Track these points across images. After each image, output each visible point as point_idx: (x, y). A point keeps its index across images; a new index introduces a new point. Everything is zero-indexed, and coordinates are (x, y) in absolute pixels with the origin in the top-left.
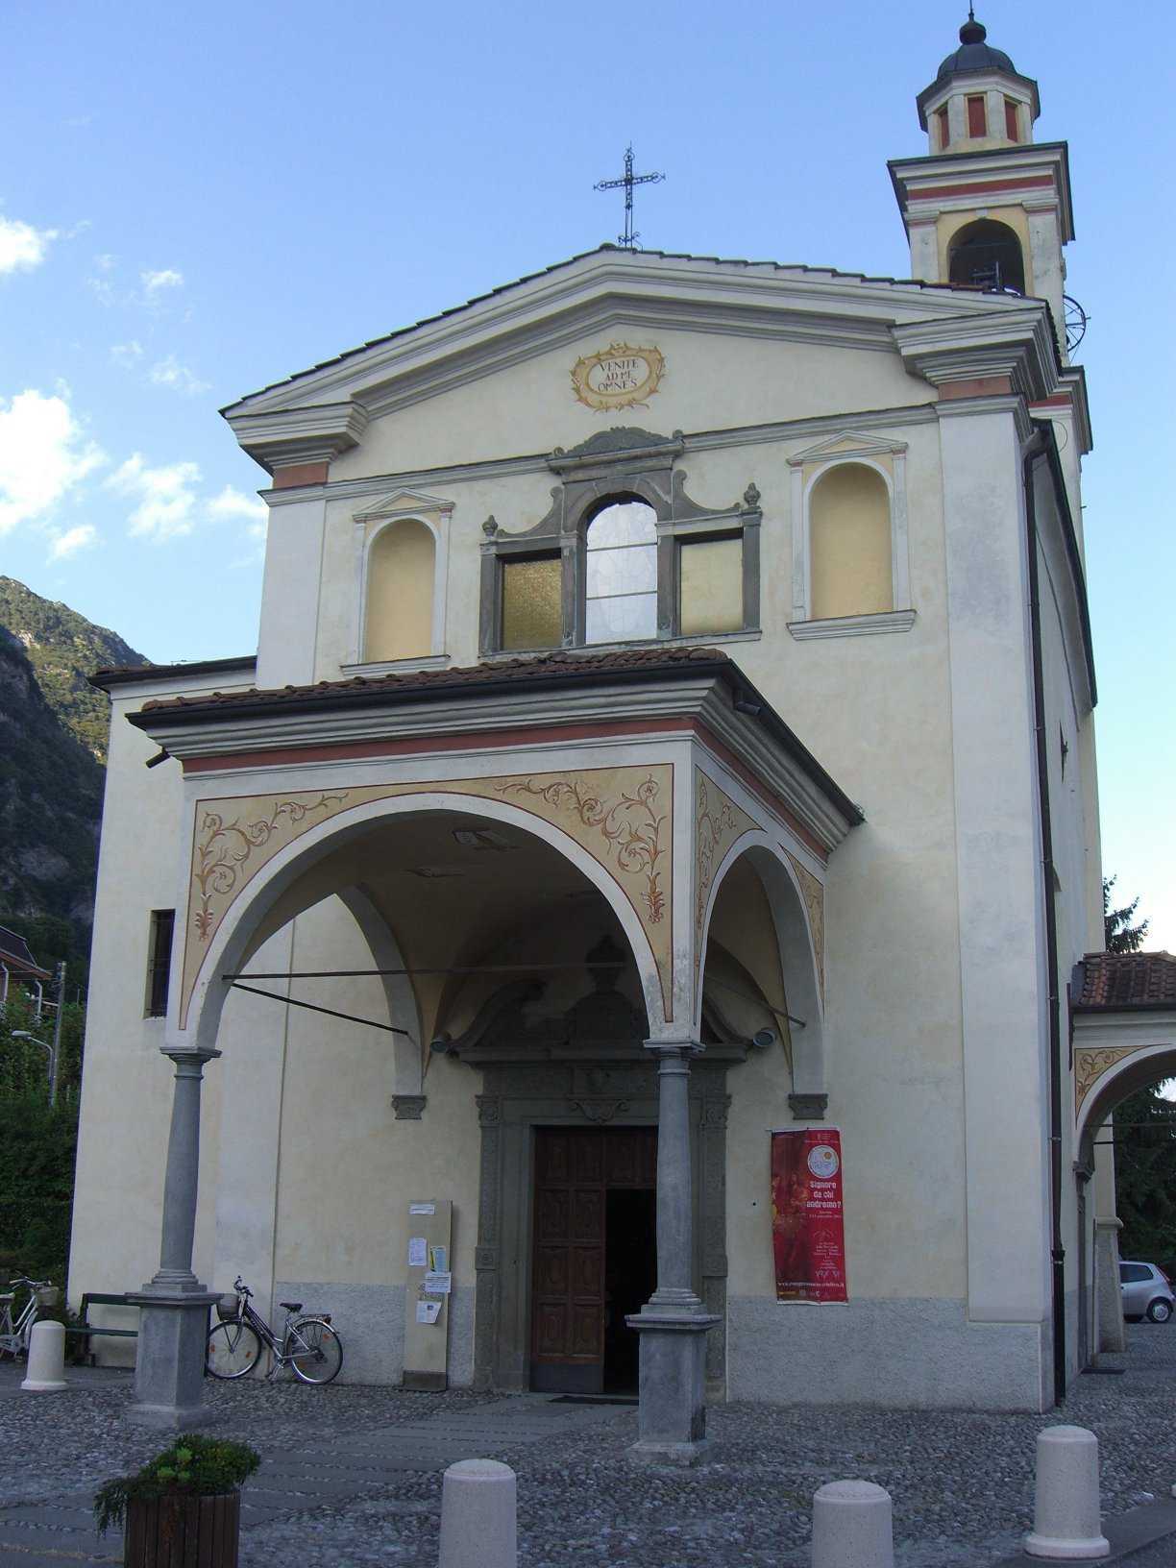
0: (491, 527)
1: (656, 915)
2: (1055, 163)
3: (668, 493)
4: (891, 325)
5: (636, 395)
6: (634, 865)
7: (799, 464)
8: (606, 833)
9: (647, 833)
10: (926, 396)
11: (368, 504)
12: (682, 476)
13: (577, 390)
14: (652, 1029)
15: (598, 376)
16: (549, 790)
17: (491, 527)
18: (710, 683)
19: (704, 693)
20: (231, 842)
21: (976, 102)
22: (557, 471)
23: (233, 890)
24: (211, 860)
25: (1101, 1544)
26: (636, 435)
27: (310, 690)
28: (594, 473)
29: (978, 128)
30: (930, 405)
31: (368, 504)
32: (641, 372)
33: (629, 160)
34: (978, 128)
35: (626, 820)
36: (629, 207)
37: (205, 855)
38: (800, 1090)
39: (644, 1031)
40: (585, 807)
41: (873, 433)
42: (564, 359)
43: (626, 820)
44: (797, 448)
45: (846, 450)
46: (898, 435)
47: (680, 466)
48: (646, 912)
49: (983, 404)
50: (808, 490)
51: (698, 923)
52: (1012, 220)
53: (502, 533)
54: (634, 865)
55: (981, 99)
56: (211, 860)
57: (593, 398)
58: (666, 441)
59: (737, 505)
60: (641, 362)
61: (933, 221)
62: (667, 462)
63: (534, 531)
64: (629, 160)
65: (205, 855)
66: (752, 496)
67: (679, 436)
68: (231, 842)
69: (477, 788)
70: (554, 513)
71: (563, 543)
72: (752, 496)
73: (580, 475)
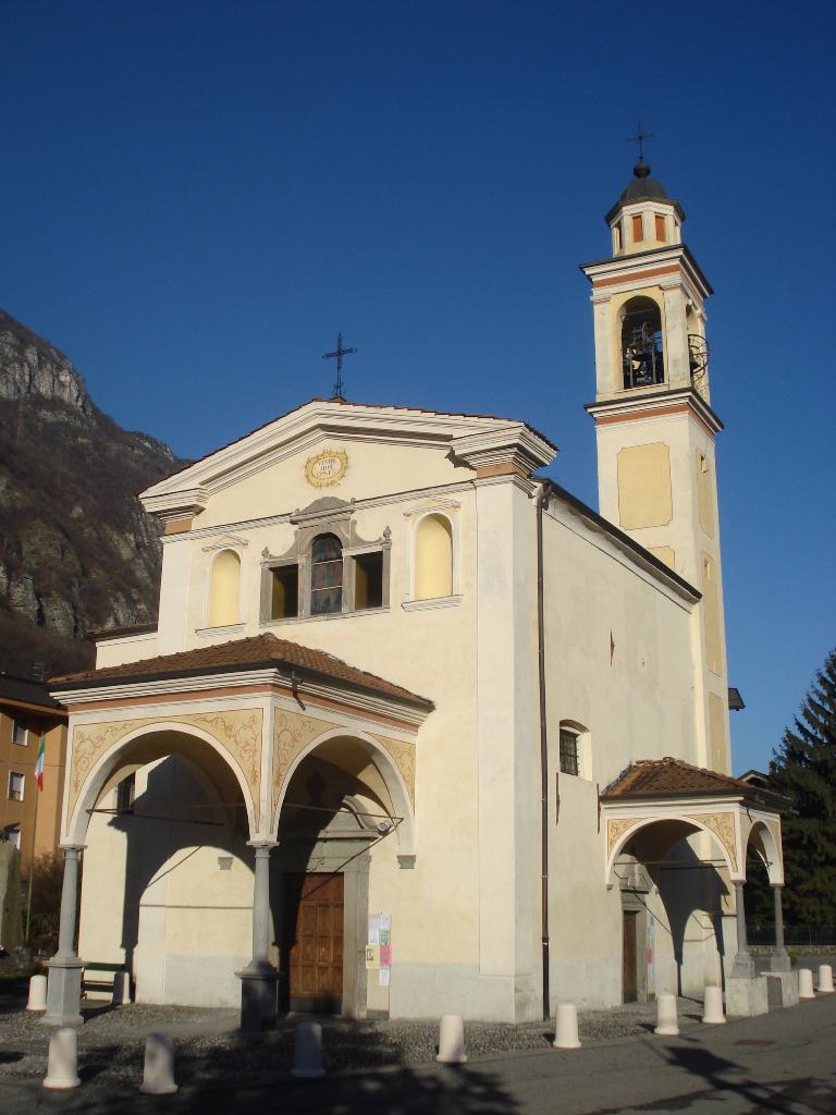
0: (265, 553)
1: (255, 777)
2: (681, 257)
3: (348, 532)
4: (449, 438)
5: (335, 479)
6: (246, 756)
7: (409, 515)
8: (236, 742)
9: (252, 742)
10: (472, 475)
11: (209, 542)
12: (355, 522)
13: (307, 476)
14: (252, 830)
15: (317, 468)
16: (217, 720)
17: (265, 553)
18: (275, 670)
19: (273, 675)
20: (87, 746)
21: (637, 218)
22: (293, 523)
23: (88, 769)
24: (79, 755)
25: (323, 1071)
26: (334, 499)
27: (116, 669)
28: (312, 522)
29: (639, 236)
30: (471, 481)
31: (209, 542)
32: (337, 465)
33: (340, 341)
34: (639, 236)
35: (245, 735)
36: (339, 368)
37: (77, 752)
38: (404, 853)
39: (248, 838)
40: (228, 728)
41: (445, 497)
42: (301, 459)
43: (245, 735)
44: (409, 506)
45: (430, 505)
46: (456, 497)
47: (353, 517)
48: (249, 775)
49: (498, 479)
50: (415, 527)
51: (277, 783)
52: (655, 295)
53: (271, 557)
54: (246, 756)
55: (640, 217)
56: (79, 755)
57: (312, 479)
58: (347, 504)
59: (380, 539)
60: (337, 460)
61: (607, 300)
62: (347, 515)
63: (286, 554)
64: (340, 341)
65: (77, 752)
66: (387, 534)
67: (355, 502)
68: (87, 746)
69: (187, 720)
70: (295, 544)
71: (298, 562)
72: (387, 534)
73: (306, 524)
